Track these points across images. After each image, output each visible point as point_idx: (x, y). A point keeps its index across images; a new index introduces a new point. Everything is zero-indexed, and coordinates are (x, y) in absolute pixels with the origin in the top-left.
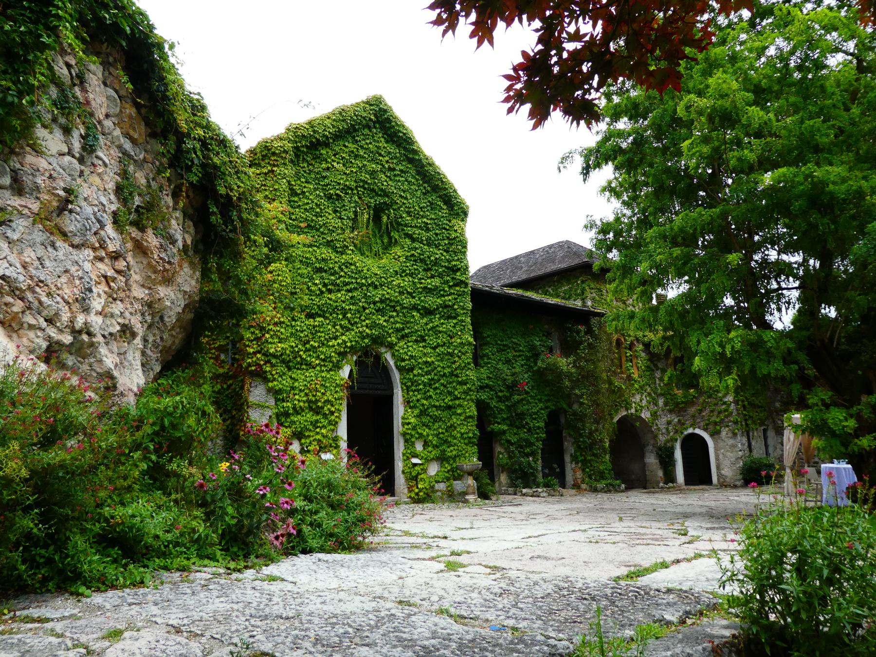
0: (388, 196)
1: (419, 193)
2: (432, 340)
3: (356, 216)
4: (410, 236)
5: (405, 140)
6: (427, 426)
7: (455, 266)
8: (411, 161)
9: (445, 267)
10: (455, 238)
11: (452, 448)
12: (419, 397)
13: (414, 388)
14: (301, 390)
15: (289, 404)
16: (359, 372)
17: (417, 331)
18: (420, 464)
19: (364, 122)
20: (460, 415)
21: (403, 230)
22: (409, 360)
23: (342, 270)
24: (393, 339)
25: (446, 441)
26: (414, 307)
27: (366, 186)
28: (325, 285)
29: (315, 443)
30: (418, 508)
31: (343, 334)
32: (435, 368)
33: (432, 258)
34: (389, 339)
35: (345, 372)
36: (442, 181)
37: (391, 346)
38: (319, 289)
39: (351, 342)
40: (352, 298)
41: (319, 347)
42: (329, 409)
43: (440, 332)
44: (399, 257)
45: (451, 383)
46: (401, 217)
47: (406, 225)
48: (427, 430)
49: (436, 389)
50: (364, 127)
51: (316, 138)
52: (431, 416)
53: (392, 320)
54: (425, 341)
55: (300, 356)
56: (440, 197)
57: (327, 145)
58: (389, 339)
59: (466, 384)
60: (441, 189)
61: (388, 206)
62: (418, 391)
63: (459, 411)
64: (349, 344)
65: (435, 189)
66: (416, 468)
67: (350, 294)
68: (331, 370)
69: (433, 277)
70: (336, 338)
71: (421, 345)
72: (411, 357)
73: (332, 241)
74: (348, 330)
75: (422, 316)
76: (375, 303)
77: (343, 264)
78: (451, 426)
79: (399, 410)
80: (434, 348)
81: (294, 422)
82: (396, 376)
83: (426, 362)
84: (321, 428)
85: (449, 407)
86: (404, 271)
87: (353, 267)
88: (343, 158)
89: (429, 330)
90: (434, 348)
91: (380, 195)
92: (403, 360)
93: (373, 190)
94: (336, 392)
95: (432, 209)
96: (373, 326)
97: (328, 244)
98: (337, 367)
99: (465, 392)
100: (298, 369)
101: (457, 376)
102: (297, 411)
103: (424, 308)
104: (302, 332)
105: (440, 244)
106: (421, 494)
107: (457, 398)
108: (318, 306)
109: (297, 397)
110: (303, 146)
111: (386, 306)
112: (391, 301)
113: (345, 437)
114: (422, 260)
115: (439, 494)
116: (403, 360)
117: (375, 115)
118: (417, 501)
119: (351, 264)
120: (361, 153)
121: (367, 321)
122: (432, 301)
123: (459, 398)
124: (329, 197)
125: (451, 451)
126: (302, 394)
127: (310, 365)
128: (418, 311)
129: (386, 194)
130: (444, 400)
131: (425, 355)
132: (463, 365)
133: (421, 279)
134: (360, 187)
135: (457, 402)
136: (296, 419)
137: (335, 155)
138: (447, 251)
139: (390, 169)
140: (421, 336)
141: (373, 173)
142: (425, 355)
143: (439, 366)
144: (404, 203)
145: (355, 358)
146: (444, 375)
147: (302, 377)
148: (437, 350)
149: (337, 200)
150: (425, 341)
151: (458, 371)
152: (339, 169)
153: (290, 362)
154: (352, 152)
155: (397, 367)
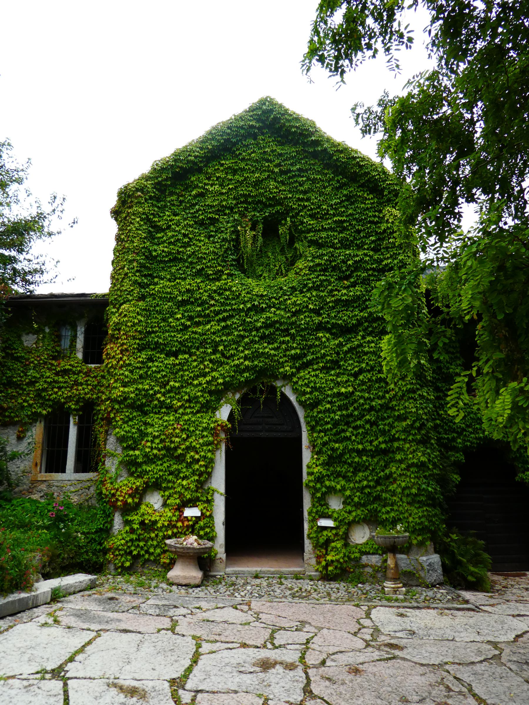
0: (281, 204)
1: (329, 189)
2: (351, 365)
3: (238, 236)
4: (312, 243)
5: (301, 134)
6: (344, 477)
7: (386, 265)
8: (315, 155)
9: (373, 269)
10: (385, 231)
11: (388, 508)
12: (326, 439)
13: (319, 428)
14: (155, 437)
15: (137, 453)
16: (244, 412)
17: (324, 355)
18: (332, 528)
19: (242, 131)
20: (401, 461)
21: (306, 238)
22: (311, 393)
23: (212, 298)
24: (288, 368)
25: (378, 498)
26: (320, 327)
27: (250, 200)
28: (190, 318)
29: (176, 496)
30: (340, 588)
31: (213, 370)
32: (355, 401)
33: (350, 262)
34: (281, 370)
35: (223, 413)
36: (361, 167)
37: (287, 378)
38: (183, 324)
39: (224, 378)
40: (224, 328)
41: (182, 387)
42: (192, 457)
43: (366, 354)
44: (301, 270)
45: (383, 419)
46: (302, 223)
47: (309, 231)
48: (343, 483)
49: (356, 428)
50: (245, 137)
51: (178, 167)
52: (350, 465)
53: (284, 346)
54: (339, 367)
55: (158, 399)
56: (363, 186)
57: (200, 170)
58: (281, 370)
59: (405, 419)
60: (361, 176)
61: (284, 215)
62: (325, 431)
63: (398, 457)
64: (220, 381)
65: (354, 178)
66: (325, 533)
67: (223, 324)
68: (198, 412)
69: (354, 285)
70: (204, 375)
71: (333, 372)
72: (314, 389)
73: (203, 269)
74: (221, 364)
75: (335, 336)
76: (257, 330)
77: (215, 291)
78: (387, 477)
79: (307, 456)
80: (356, 375)
81: (147, 472)
82: (301, 413)
83: (339, 394)
84: (183, 479)
85: (385, 452)
86: (305, 285)
87: (228, 293)
88: (218, 178)
89: (346, 352)
90: (356, 375)
91: (271, 206)
92: (304, 393)
93: (260, 202)
94: (203, 437)
95: (352, 203)
96: (256, 355)
97: (199, 273)
98: (210, 407)
99: (404, 431)
100: (156, 413)
101: (393, 409)
102: (150, 460)
103: (334, 325)
104: (159, 372)
105: (364, 244)
106: (330, 568)
107: (394, 439)
108: (180, 343)
109: (149, 444)
110: (166, 180)
111: (272, 331)
112: (281, 324)
113: (222, 490)
114: (334, 268)
115: (369, 570)
116: (304, 393)
117: (258, 121)
118: (326, 577)
119: (226, 290)
120: (242, 165)
121: (247, 352)
122: (347, 317)
123: (398, 439)
124: (201, 224)
125: (388, 512)
126: (157, 441)
127: (170, 407)
128: (329, 330)
129: (279, 202)
130: (371, 442)
131: (338, 384)
132: (400, 393)
133: (332, 291)
134: (242, 203)
135: (396, 444)
136: (148, 469)
137: (209, 179)
138: (376, 250)
139: (282, 172)
140: (332, 361)
141: (257, 183)
142: (338, 384)
143: (362, 397)
144: (305, 207)
145: (238, 396)
146: (372, 408)
147: (156, 424)
148: (361, 377)
149: (211, 224)
150: (339, 367)
151: (394, 403)
152: (214, 189)
153: (141, 407)
154: (229, 168)
155: (301, 403)
